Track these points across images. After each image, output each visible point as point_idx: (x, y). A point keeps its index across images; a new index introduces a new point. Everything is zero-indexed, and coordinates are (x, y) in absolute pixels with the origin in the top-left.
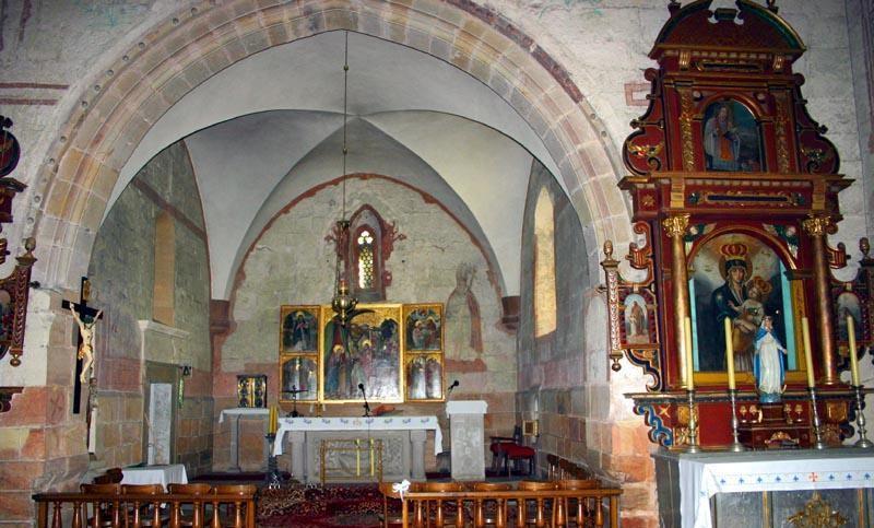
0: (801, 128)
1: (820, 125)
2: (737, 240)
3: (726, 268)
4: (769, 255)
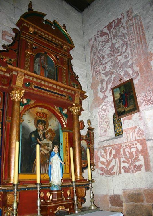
0: (71, 74)
1: (77, 75)
2: (43, 111)
3: (37, 123)
4: (56, 120)
